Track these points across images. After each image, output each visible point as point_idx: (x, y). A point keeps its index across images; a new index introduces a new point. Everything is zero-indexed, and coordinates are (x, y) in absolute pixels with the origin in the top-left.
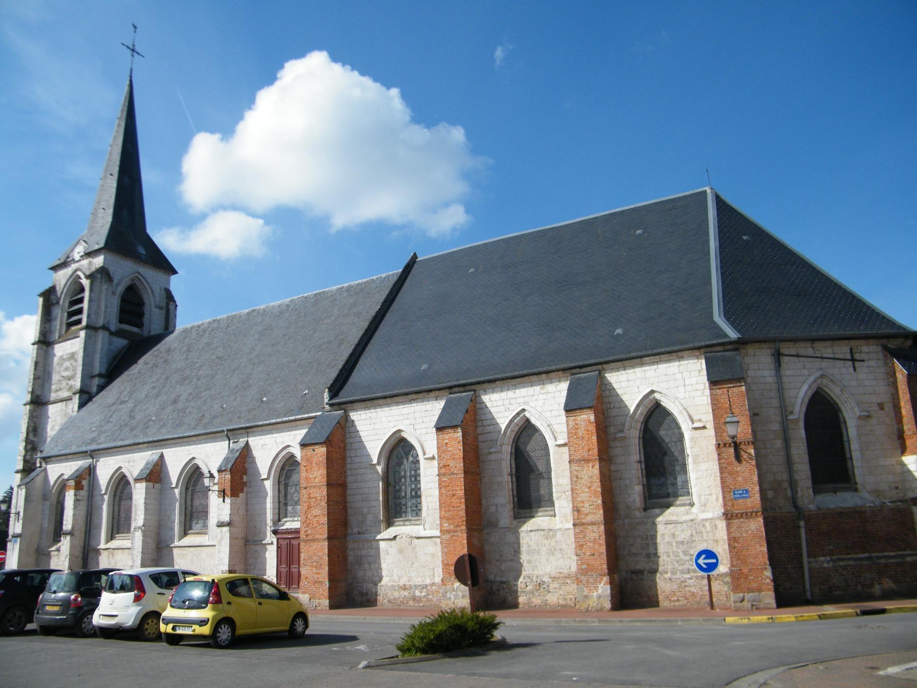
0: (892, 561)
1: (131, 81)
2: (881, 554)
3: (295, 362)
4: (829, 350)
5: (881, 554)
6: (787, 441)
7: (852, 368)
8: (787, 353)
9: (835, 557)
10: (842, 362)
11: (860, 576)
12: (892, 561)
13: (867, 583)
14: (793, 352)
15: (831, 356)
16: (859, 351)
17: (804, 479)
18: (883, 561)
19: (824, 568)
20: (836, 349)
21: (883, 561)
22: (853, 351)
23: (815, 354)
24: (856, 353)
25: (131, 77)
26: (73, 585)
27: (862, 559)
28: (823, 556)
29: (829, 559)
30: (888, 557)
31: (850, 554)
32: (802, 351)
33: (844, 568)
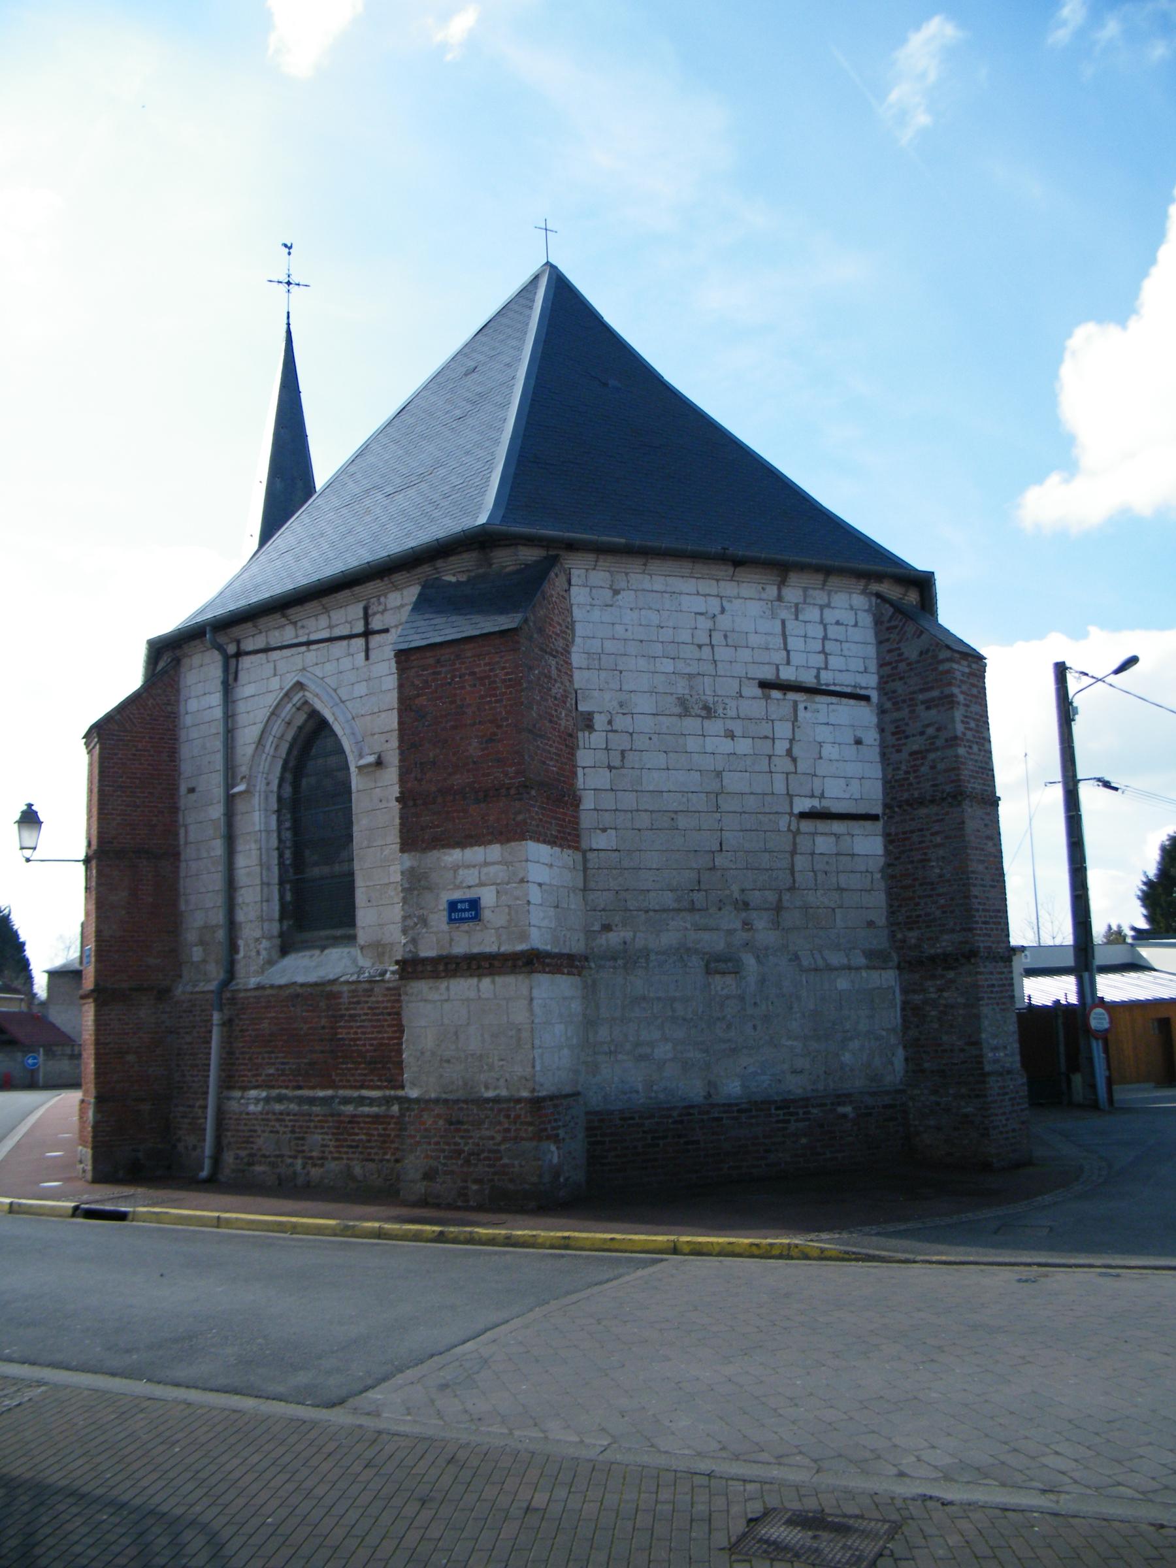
0: (366, 1109)
1: (289, 333)
2: (356, 1094)
3: (567, 627)
4: (323, 621)
5: (356, 1094)
6: (230, 840)
7: (363, 655)
8: (250, 648)
9: (274, 1092)
10: (345, 643)
11: (303, 1139)
12: (366, 1109)
13: (314, 1154)
14: (259, 642)
15: (325, 634)
16: (381, 608)
17: (251, 921)
18: (349, 1109)
19: (248, 1114)
20: (338, 616)
21: (349, 1109)
22: (370, 612)
23: (297, 637)
24: (375, 614)
25: (288, 324)
26: (336, 941)
27: (312, 1101)
28: (256, 1087)
29: (264, 1094)
30: (361, 1101)
31: (299, 1088)
32: (276, 638)
33: (280, 1117)
